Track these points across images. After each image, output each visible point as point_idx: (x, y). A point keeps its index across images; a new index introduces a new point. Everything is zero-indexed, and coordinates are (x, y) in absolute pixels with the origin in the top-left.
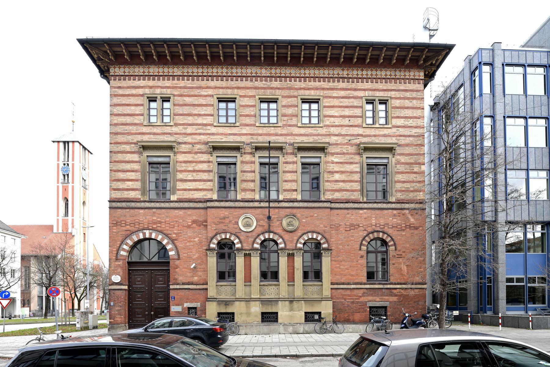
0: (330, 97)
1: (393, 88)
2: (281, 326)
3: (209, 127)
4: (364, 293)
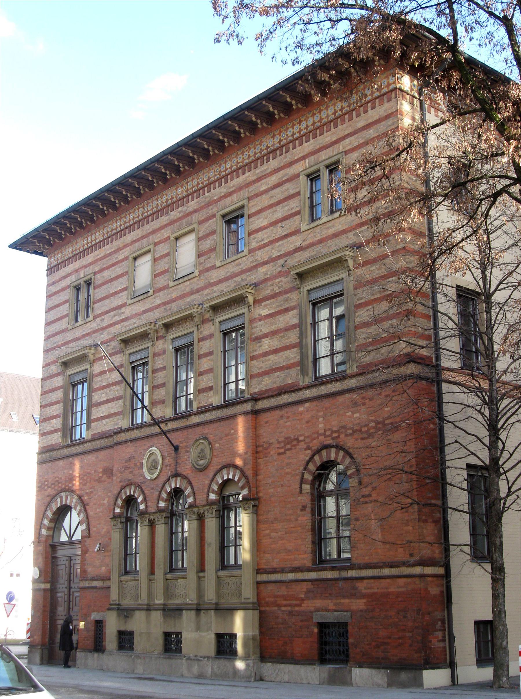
0: (257, 195)
1: (347, 132)
2: (184, 661)
3: (123, 310)
4: (308, 591)
